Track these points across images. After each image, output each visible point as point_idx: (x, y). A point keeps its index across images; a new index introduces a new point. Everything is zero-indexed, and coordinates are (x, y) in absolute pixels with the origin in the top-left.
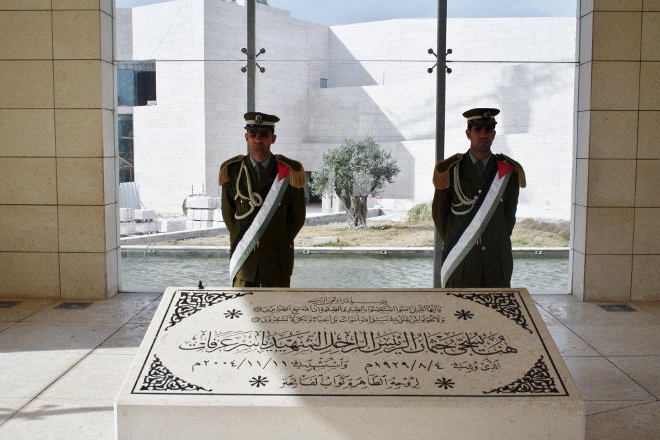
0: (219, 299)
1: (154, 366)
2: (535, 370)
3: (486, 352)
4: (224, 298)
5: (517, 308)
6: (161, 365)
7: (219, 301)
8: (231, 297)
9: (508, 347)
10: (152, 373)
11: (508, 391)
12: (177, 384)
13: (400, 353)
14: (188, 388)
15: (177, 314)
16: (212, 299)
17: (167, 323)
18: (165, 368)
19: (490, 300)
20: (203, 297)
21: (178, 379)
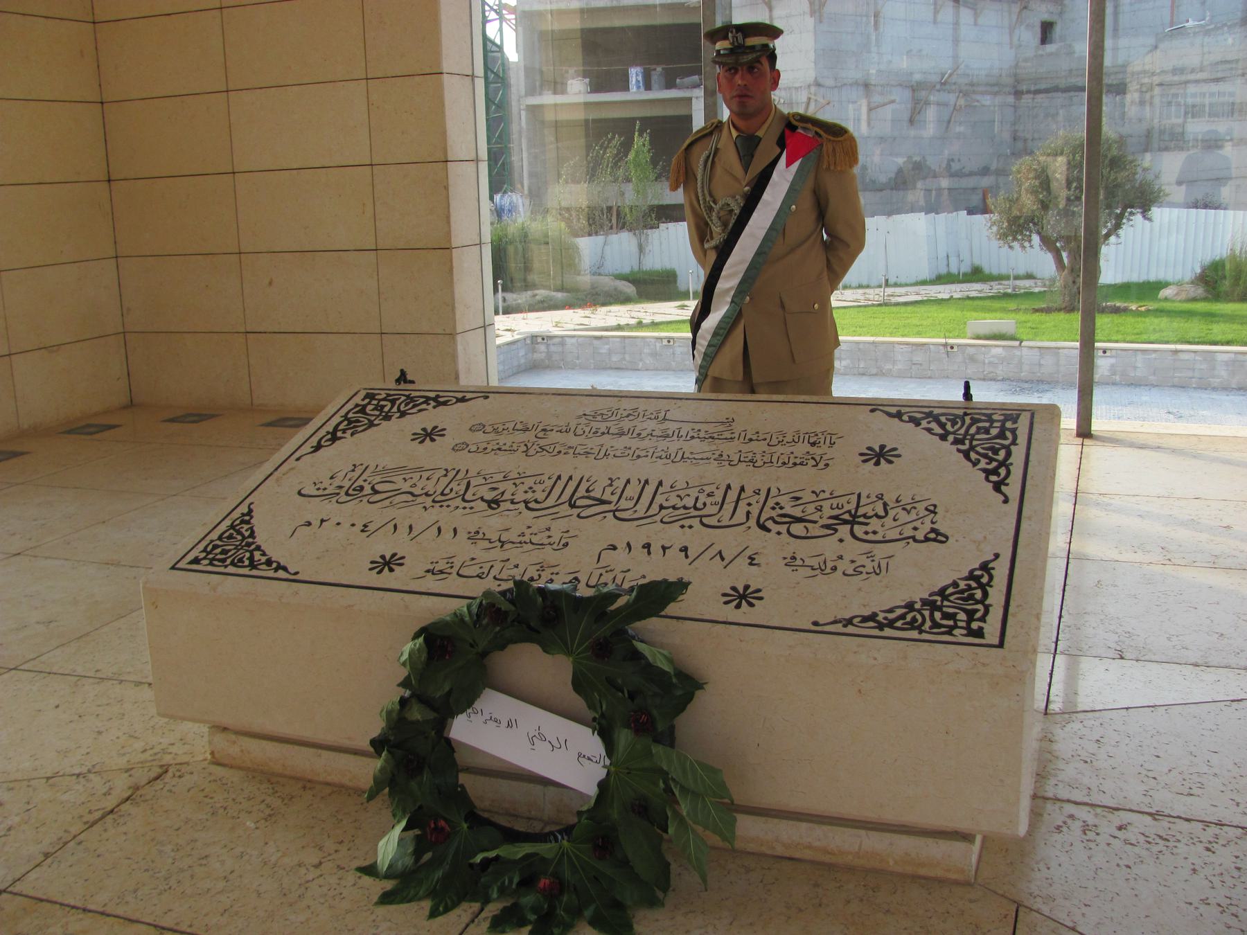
0: (891, 616)
1: (1003, 471)
2: (962, 585)
3: (878, 537)
4: (880, 618)
6: (988, 473)
7: (891, 611)
8: (865, 619)
9: (933, 530)
10: (1002, 453)
11: (871, 624)
12: (942, 426)
13: (690, 527)
14: (919, 416)
15: (982, 587)
16: (909, 618)
17: (307, 448)
18: (975, 464)
20: (928, 623)
21: (943, 437)
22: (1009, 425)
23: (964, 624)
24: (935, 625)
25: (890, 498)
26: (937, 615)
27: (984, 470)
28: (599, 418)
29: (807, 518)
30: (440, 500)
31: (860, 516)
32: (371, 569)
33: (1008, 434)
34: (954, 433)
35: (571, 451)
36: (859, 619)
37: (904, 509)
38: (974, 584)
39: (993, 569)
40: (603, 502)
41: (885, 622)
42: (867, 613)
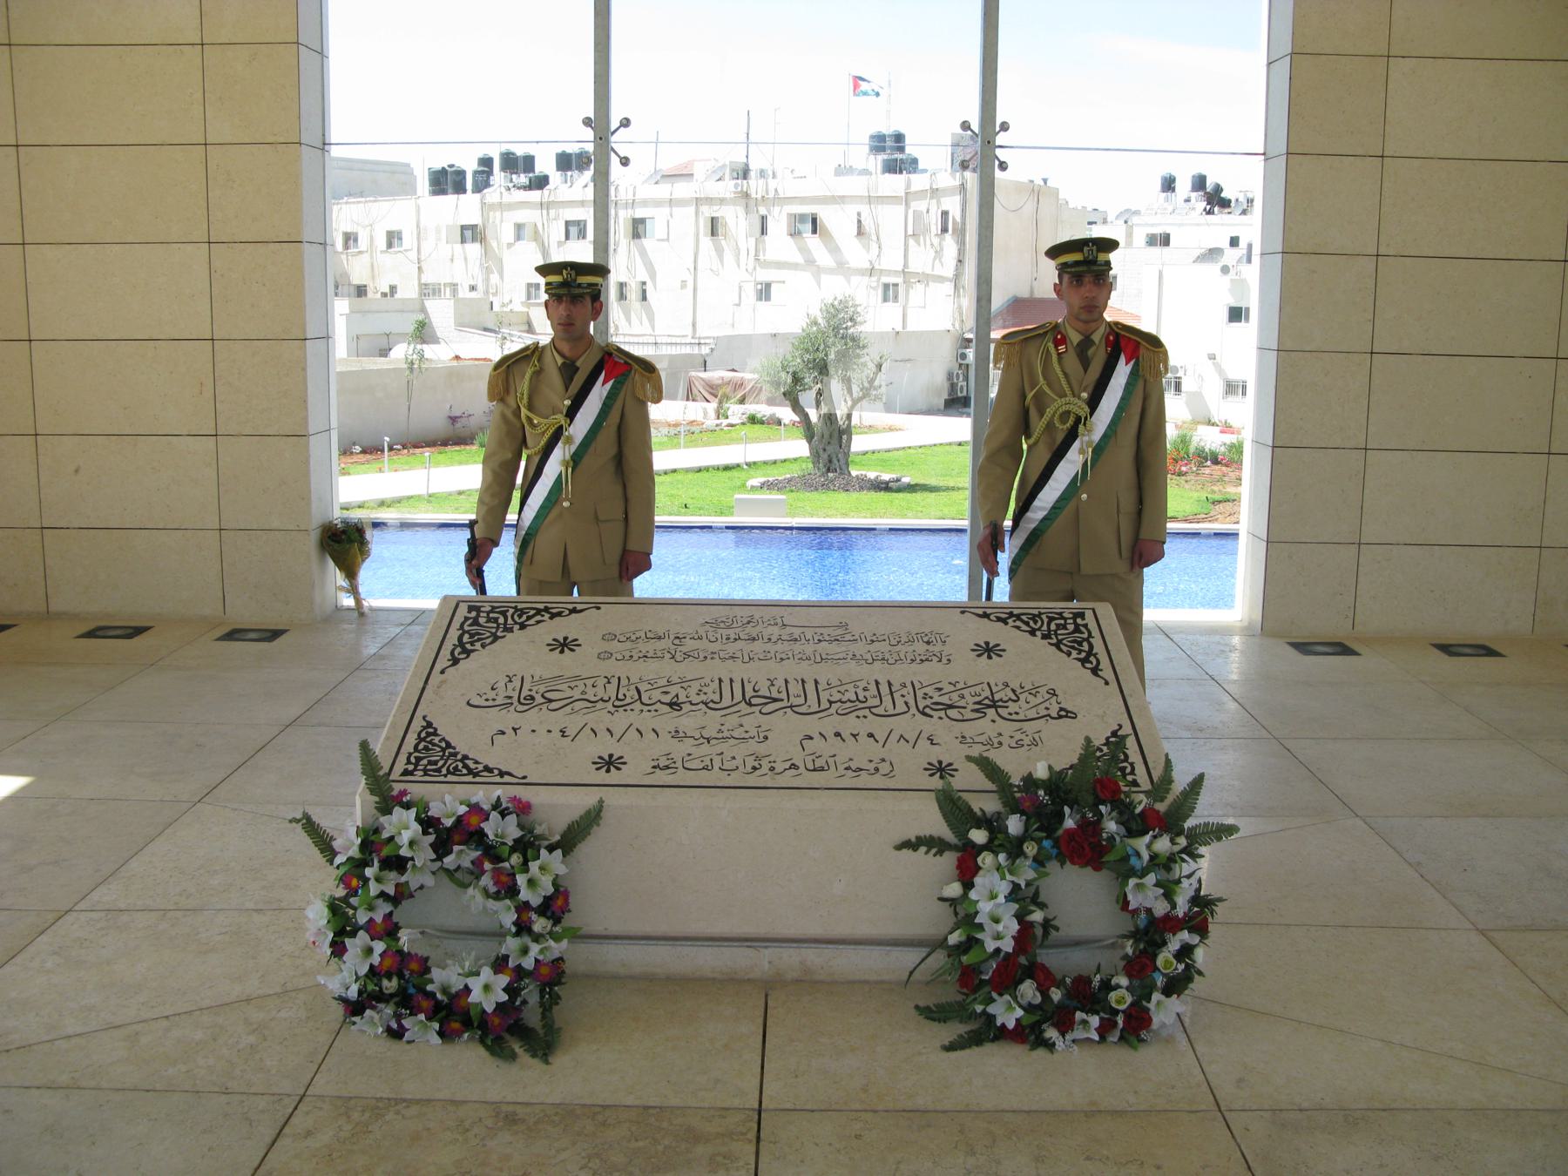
0: (538, 618)
3: (1021, 717)
5: (1087, 640)
6: (435, 734)
7: (538, 622)
8: (559, 614)
9: (1061, 709)
10: (421, 746)
12: (465, 766)
16: (524, 617)
20: (509, 614)
21: (465, 757)
22: (411, 767)
23: (482, 614)
25: (1015, 685)
26: (501, 620)
27: (436, 735)
30: (620, 704)
31: (998, 701)
33: (413, 760)
34: (456, 761)
36: (564, 614)
37: (1030, 693)
39: (449, 660)
40: (775, 700)
41: (543, 613)
42: (557, 619)
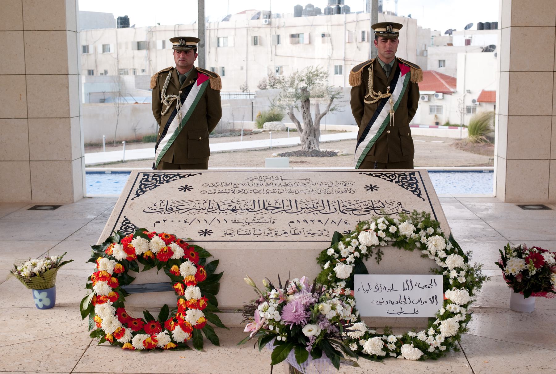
0: (175, 178)
4: (178, 177)
5: (416, 183)
7: (174, 180)
16: (168, 178)
19: (395, 177)
20: (162, 177)
24: (159, 177)
28: (255, 180)
29: (357, 209)
32: (379, 188)
34: (394, 179)
35: (252, 191)
38: (144, 189)
